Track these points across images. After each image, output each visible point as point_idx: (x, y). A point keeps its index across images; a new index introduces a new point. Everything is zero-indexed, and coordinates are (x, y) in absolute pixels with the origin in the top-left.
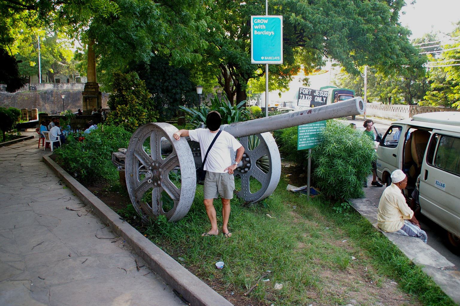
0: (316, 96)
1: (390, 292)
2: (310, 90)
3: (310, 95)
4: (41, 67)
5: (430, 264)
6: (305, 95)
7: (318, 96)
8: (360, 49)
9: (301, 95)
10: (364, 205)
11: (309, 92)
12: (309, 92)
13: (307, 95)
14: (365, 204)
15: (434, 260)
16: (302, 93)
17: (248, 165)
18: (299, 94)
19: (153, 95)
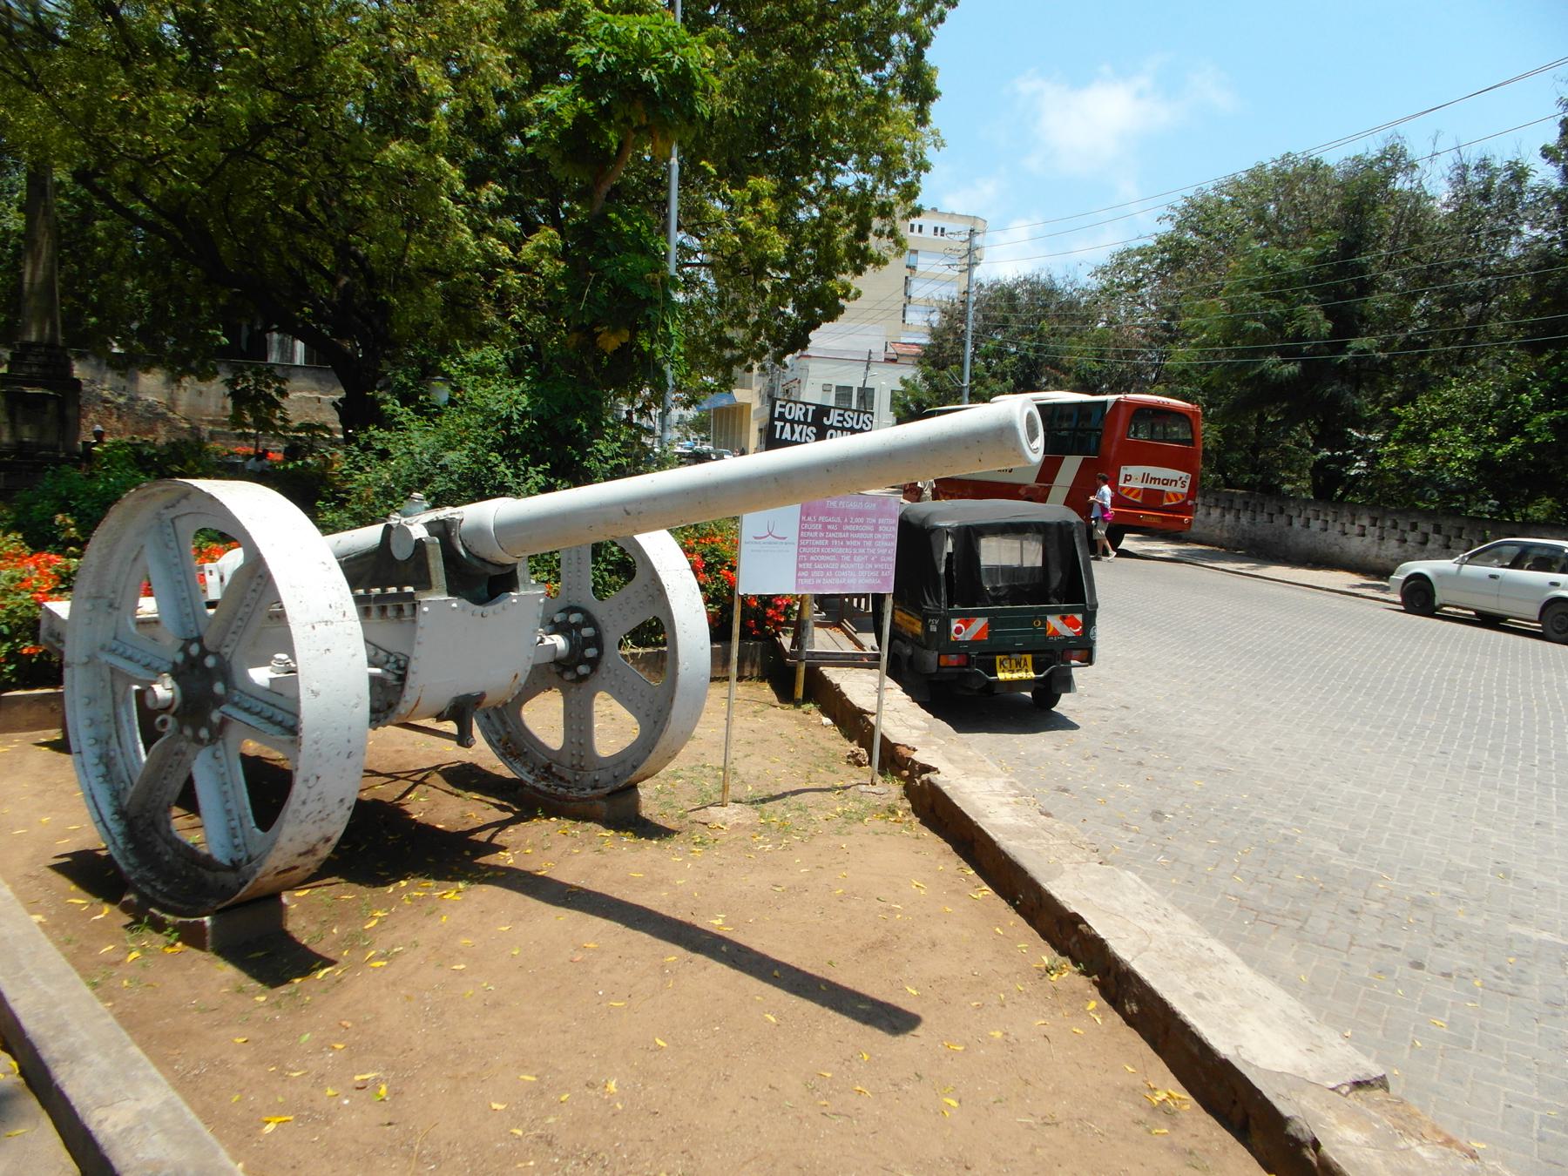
0: (831, 427)
1: (692, 769)
2: (811, 408)
3: (809, 425)
4: (581, 477)
5: (1296, 1068)
6: (792, 422)
7: (836, 429)
8: (1473, 249)
9: (779, 424)
10: (1002, 804)
11: (806, 415)
12: (806, 415)
13: (799, 422)
14: (1004, 800)
15: (1303, 1048)
16: (782, 417)
17: (587, 632)
18: (772, 419)
19: (926, 626)
